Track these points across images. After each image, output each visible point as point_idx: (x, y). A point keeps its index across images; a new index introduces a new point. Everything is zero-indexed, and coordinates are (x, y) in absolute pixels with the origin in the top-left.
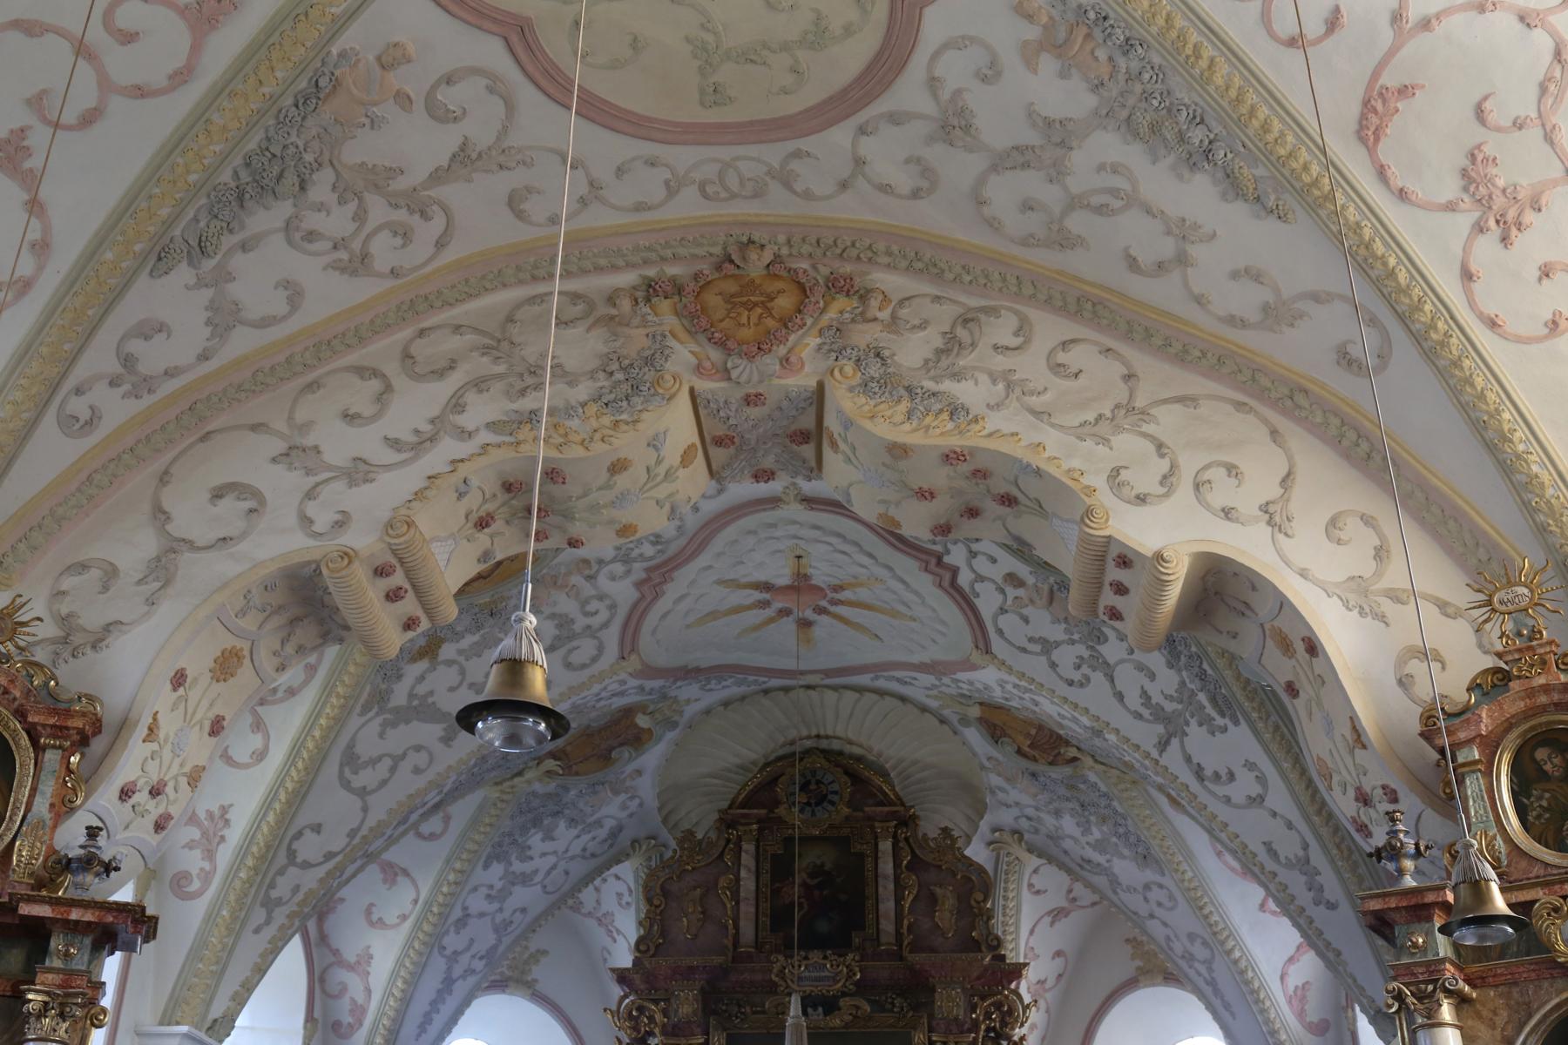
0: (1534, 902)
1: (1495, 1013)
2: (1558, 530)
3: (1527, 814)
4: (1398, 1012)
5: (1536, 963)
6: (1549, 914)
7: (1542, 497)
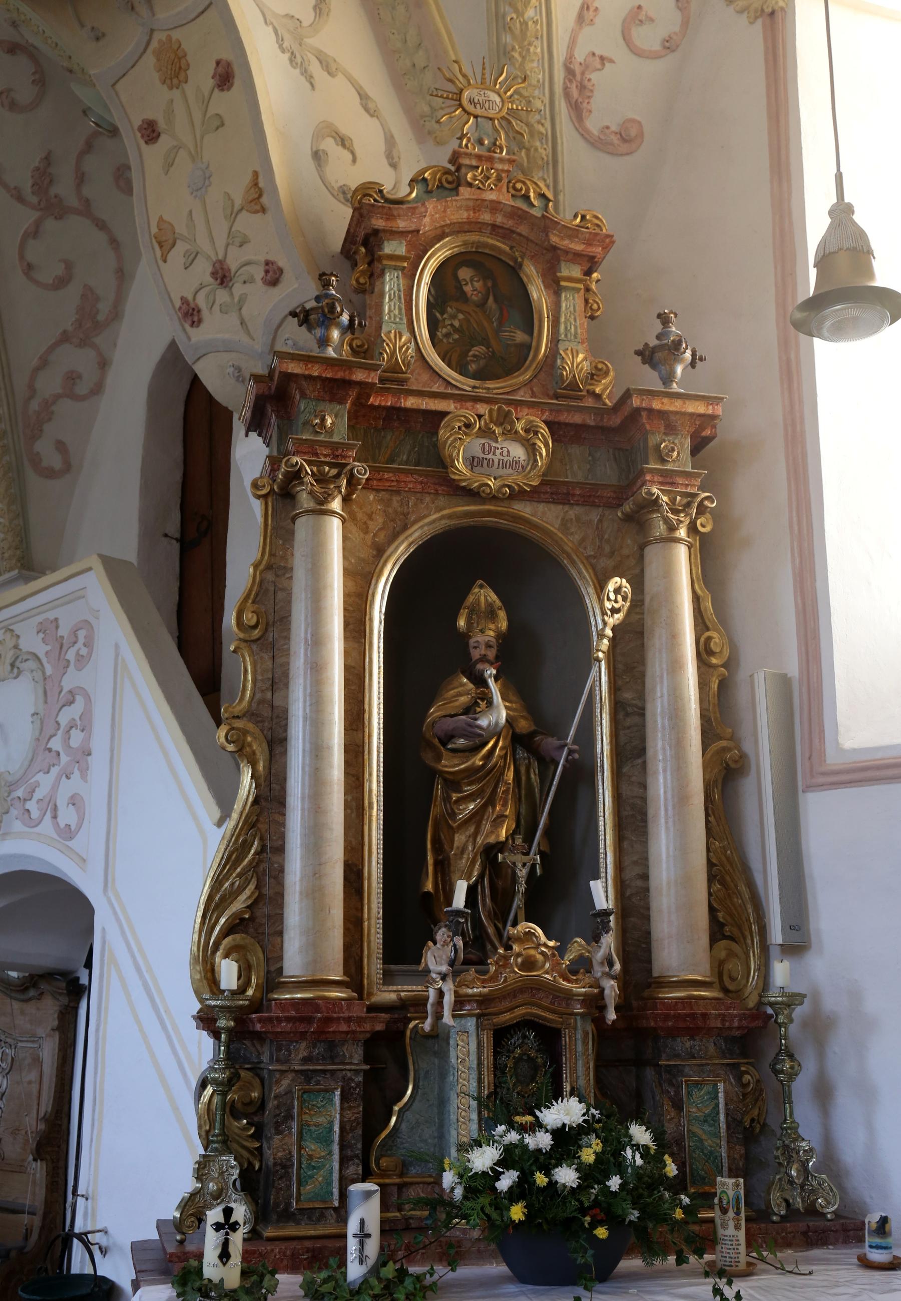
0: (444, 414)
1: (370, 517)
2: (520, 59)
4: (265, 497)
5: (426, 476)
6: (459, 428)
7: (520, 14)
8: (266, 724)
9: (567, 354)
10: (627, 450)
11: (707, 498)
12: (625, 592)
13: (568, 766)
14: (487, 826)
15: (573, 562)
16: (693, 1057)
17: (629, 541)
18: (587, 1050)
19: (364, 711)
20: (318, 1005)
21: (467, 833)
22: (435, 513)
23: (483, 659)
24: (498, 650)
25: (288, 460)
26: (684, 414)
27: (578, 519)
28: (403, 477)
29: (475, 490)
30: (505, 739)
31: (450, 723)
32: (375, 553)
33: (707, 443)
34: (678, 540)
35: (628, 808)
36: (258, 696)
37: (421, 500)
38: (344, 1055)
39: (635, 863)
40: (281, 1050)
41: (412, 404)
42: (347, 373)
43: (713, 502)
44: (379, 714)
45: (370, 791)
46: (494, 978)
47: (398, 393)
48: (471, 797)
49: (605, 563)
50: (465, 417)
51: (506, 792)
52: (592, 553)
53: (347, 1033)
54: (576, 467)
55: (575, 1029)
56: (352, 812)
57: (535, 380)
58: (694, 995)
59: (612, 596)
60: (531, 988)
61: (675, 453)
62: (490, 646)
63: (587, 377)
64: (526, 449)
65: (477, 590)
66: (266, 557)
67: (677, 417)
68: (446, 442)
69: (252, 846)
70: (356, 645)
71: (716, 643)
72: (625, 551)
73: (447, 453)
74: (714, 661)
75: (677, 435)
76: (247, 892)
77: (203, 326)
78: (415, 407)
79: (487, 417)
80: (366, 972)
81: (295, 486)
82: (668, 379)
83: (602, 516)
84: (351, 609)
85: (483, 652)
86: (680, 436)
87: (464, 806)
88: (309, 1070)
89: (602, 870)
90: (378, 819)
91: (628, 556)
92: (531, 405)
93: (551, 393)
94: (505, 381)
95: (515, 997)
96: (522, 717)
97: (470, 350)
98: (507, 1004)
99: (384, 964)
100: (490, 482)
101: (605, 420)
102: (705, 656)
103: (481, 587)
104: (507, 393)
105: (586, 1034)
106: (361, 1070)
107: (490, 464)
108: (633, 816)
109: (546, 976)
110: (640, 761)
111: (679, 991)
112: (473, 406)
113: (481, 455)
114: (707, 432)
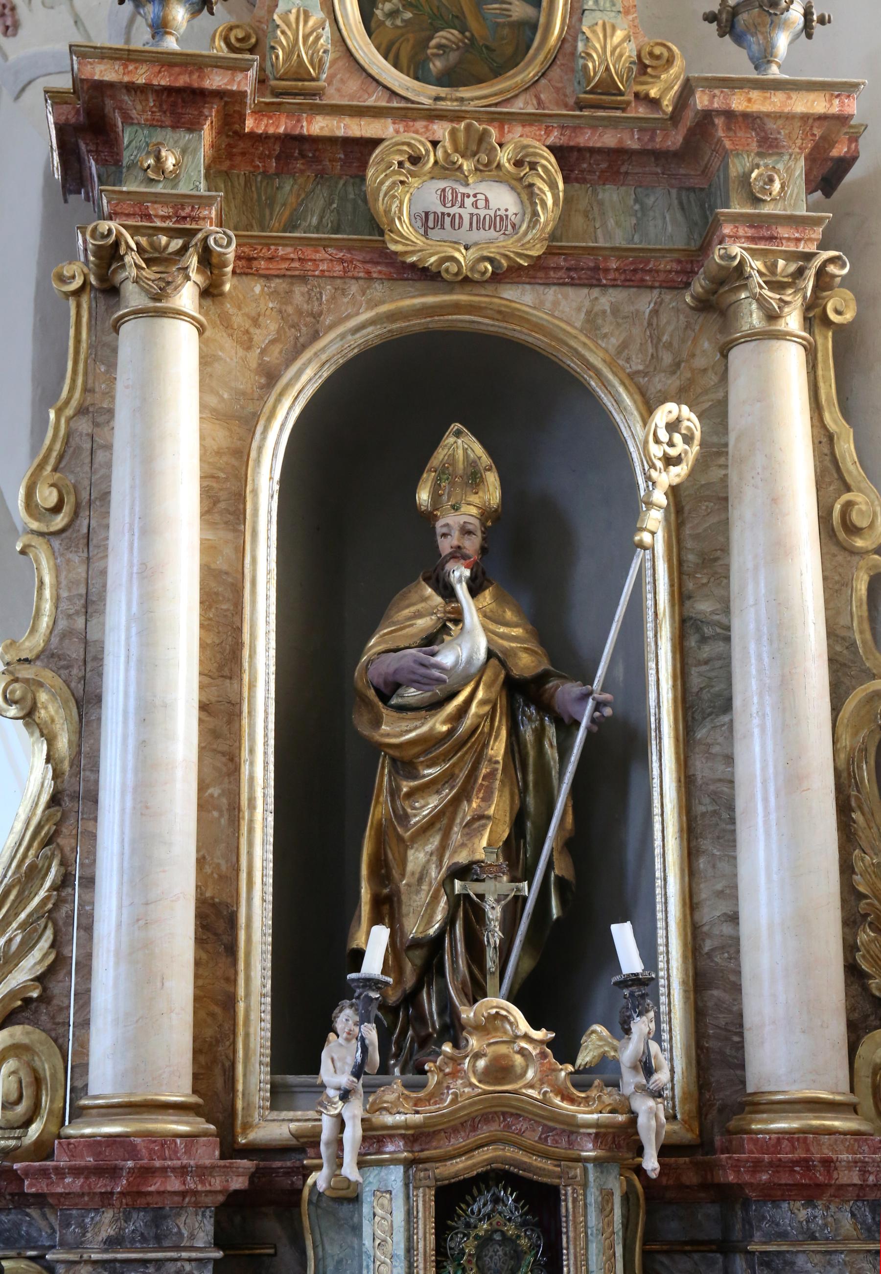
0: (375, 143)
1: (256, 322)
3: (370, 21)
4: (77, 293)
5: (349, 249)
6: (401, 164)
8: (75, 671)
9: (594, 32)
10: (702, 189)
11: (832, 260)
12: (688, 428)
13: (595, 729)
14: (457, 835)
15: (605, 384)
16: (813, 1238)
17: (706, 345)
18: (611, 1223)
19: (242, 644)
20: (134, 1146)
21: (429, 848)
22: (367, 310)
23: (458, 554)
24: (484, 539)
25: (95, 229)
26: (789, 117)
27: (615, 311)
28: (309, 253)
29: (434, 269)
30: (489, 687)
31: (391, 663)
32: (263, 381)
33: (846, 170)
34: (782, 336)
35: (706, 800)
36: (62, 624)
37: (344, 291)
38: (180, 1234)
39: (720, 894)
40: (68, 1225)
41: (322, 128)
42: (195, 77)
43: (843, 266)
44: (267, 650)
45: (252, 779)
46: (436, 1095)
47: (295, 112)
48: (433, 786)
49: (659, 383)
50: (409, 144)
51: (491, 776)
52: (641, 367)
53: (183, 1194)
54: (611, 223)
55: (585, 1186)
56: (221, 816)
57: (543, 81)
58: (812, 1126)
59: (663, 436)
60: (504, 1114)
61: (777, 186)
62: (470, 532)
63: (630, 70)
64: (519, 194)
65: (451, 440)
66: (77, 394)
67: (780, 122)
68: (379, 189)
69: (46, 874)
70: (230, 536)
71: (861, 511)
72: (700, 362)
73: (381, 207)
74: (859, 543)
75: (780, 155)
76: (36, 954)
77: (22, 32)
78: (326, 133)
79: (447, 143)
80: (240, 1087)
81: (115, 271)
82: (764, 58)
83: (659, 303)
84: (222, 475)
85: (455, 542)
86: (786, 157)
87: (422, 802)
88: (115, 1261)
89: (659, 907)
90: (265, 826)
91: (705, 370)
92: (527, 120)
93: (571, 101)
94: (492, 86)
95: (474, 1129)
96: (526, 650)
97: (431, 38)
98: (459, 1141)
99: (272, 1073)
100: (457, 255)
101: (658, 139)
102: (842, 535)
103: (458, 434)
104: (496, 105)
105: (607, 1196)
106: (209, 1259)
107: (456, 222)
108: (715, 813)
109: (530, 1092)
110: (725, 719)
111: (785, 1119)
112: (426, 127)
113: (440, 209)
114: (840, 150)
